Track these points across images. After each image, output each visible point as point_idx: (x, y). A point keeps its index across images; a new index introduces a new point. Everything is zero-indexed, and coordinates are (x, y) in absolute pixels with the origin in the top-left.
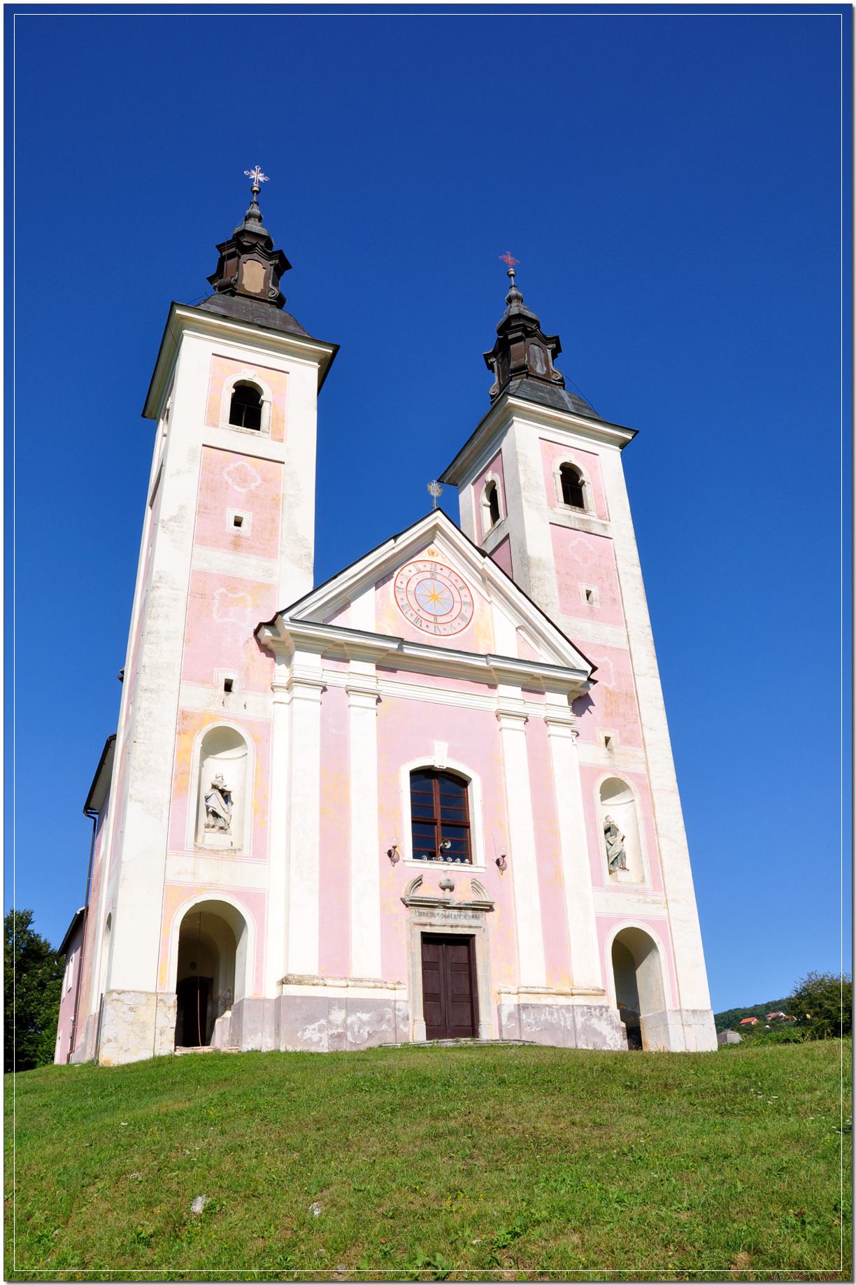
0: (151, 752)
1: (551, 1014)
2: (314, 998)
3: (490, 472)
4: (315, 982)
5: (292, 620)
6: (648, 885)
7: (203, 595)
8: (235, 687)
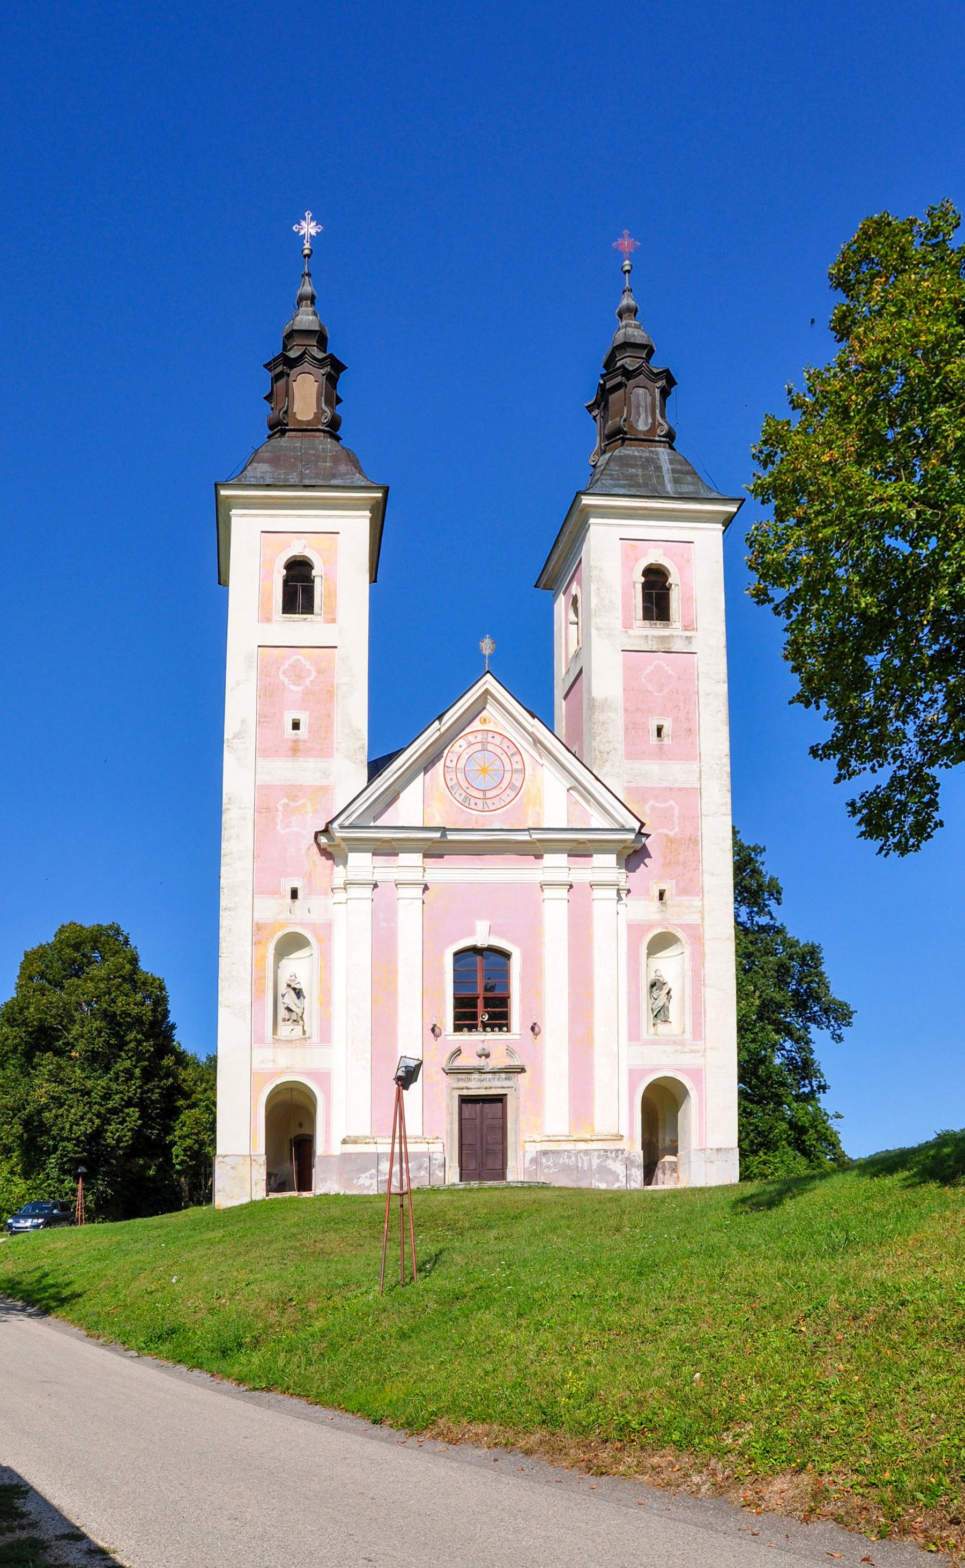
0: (234, 964)
1: (569, 1157)
2: (367, 1153)
3: (575, 583)
4: (367, 1141)
5: (342, 827)
6: (688, 1035)
7: (268, 809)
8: (300, 894)
